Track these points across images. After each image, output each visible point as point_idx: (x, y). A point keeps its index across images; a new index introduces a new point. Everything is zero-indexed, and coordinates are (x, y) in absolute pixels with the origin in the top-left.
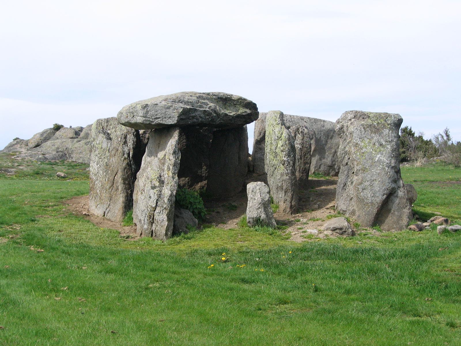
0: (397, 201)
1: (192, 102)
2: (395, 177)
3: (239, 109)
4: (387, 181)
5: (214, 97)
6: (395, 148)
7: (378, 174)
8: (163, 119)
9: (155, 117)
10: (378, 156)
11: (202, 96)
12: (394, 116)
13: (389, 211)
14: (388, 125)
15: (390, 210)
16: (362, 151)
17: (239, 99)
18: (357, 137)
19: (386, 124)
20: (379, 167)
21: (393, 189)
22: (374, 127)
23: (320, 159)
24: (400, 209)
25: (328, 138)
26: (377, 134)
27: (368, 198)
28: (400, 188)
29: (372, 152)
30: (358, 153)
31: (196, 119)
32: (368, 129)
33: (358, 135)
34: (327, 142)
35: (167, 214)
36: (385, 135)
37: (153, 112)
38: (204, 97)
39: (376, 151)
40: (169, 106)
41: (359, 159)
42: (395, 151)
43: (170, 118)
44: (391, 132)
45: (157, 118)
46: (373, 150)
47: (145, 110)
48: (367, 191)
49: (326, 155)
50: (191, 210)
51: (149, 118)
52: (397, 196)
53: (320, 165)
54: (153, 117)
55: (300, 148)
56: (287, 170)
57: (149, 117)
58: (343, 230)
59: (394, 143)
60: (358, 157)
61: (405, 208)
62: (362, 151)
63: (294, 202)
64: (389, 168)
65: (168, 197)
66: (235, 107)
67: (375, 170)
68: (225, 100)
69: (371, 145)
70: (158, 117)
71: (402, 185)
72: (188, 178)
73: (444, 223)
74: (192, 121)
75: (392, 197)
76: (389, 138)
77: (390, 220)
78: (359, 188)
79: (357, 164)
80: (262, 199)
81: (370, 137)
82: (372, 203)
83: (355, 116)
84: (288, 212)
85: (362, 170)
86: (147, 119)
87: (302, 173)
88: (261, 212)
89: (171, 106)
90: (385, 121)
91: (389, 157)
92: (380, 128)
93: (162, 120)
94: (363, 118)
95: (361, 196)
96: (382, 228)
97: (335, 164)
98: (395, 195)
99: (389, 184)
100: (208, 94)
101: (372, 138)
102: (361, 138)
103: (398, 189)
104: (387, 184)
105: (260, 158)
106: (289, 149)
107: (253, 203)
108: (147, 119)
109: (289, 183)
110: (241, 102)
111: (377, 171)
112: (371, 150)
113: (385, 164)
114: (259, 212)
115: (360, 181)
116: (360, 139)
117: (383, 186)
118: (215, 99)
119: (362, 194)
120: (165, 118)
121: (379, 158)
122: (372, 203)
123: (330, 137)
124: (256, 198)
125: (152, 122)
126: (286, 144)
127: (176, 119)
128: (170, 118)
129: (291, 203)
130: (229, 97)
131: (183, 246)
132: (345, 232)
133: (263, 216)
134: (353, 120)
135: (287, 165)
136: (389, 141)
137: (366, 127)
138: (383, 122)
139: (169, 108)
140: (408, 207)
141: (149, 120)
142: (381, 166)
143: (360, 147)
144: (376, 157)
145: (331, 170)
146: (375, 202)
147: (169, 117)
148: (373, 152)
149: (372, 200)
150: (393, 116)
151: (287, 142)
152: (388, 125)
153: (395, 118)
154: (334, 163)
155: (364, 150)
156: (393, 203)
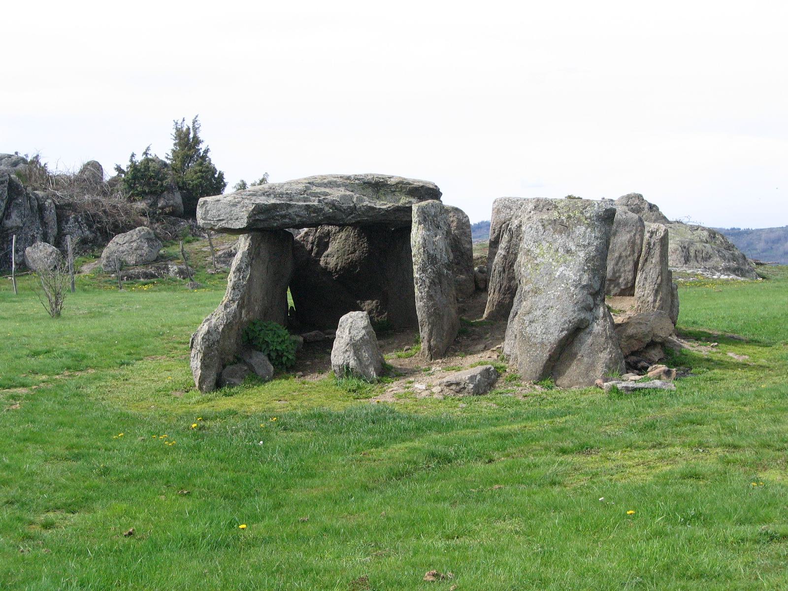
0: (589, 340)
1: (291, 193)
2: (588, 302)
3: (401, 198)
4: (571, 309)
6: (594, 257)
8: (228, 221)
9: (218, 219)
10: (561, 269)
11: (335, 182)
12: (598, 204)
13: (573, 356)
14: (586, 219)
15: (576, 354)
16: (535, 262)
17: (398, 183)
18: (531, 240)
20: (559, 287)
21: (581, 321)
22: (562, 223)
24: (593, 353)
26: (563, 234)
27: (537, 336)
28: (598, 319)
29: (551, 264)
30: (529, 266)
31: (290, 219)
32: (549, 227)
33: (532, 237)
35: (201, 360)
36: (577, 235)
37: (214, 211)
38: (338, 183)
39: (558, 262)
40: (235, 202)
41: (530, 274)
42: (593, 260)
43: (237, 219)
44: (589, 230)
45: (220, 220)
46: (553, 259)
47: (204, 209)
48: (536, 325)
50: (266, 353)
51: (210, 220)
52: (590, 333)
54: (215, 219)
55: (504, 255)
56: (421, 293)
57: (209, 218)
58: (462, 386)
59: (592, 248)
60: (529, 271)
61: (602, 352)
62: (535, 262)
63: (434, 341)
64: (576, 287)
65: (203, 335)
66: (394, 195)
67: (553, 291)
68: (378, 186)
69: (552, 251)
70: (221, 218)
71: (601, 315)
72: (376, 301)
73: (664, 377)
75: (582, 334)
76: (585, 241)
77: (574, 371)
78: (525, 320)
79: (526, 282)
80: (351, 337)
82: (542, 343)
83: (535, 207)
84: (426, 355)
85: (533, 291)
86: (206, 222)
87: (504, 294)
88: (349, 357)
89: (239, 202)
90: (582, 213)
91: (579, 271)
92: (571, 225)
93: (228, 223)
94: (548, 209)
95: (526, 333)
96: (558, 382)
97: (620, 277)
98: (587, 330)
99: (574, 313)
100: (348, 178)
101: (555, 240)
102: (537, 242)
103: (593, 320)
104: (571, 313)
106: (423, 261)
107: (339, 343)
108: (206, 222)
109: (424, 312)
110: (401, 187)
111: (556, 293)
112: (551, 260)
113: (570, 281)
114: (346, 356)
115: (528, 309)
116: (534, 242)
117: (562, 317)
118: (358, 185)
119: (528, 329)
120: (231, 219)
121: (562, 273)
122: (542, 343)
124: (344, 336)
125: (214, 225)
126: (419, 253)
127: (246, 221)
128: (237, 219)
129: (429, 341)
130: (381, 180)
131: (223, 403)
132: (464, 388)
133: (352, 363)
134: (532, 212)
135: (420, 286)
136: (584, 245)
138: (578, 215)
139: (235, 205)
140: (608, 350)
141: (210, 223)
142: (563, 285)
143: (533, 255)
144: (557, 270)
145: (612, 286)
146: (546, 342)
147: (235, 218)
148: (554, 263)
149: (542, 339)
150: (596, 206)
151: (422, 250)
152: (586, 219)
153: (599, 207)
154: (617, 274)
155: (539, 260)
156: (582, 344)
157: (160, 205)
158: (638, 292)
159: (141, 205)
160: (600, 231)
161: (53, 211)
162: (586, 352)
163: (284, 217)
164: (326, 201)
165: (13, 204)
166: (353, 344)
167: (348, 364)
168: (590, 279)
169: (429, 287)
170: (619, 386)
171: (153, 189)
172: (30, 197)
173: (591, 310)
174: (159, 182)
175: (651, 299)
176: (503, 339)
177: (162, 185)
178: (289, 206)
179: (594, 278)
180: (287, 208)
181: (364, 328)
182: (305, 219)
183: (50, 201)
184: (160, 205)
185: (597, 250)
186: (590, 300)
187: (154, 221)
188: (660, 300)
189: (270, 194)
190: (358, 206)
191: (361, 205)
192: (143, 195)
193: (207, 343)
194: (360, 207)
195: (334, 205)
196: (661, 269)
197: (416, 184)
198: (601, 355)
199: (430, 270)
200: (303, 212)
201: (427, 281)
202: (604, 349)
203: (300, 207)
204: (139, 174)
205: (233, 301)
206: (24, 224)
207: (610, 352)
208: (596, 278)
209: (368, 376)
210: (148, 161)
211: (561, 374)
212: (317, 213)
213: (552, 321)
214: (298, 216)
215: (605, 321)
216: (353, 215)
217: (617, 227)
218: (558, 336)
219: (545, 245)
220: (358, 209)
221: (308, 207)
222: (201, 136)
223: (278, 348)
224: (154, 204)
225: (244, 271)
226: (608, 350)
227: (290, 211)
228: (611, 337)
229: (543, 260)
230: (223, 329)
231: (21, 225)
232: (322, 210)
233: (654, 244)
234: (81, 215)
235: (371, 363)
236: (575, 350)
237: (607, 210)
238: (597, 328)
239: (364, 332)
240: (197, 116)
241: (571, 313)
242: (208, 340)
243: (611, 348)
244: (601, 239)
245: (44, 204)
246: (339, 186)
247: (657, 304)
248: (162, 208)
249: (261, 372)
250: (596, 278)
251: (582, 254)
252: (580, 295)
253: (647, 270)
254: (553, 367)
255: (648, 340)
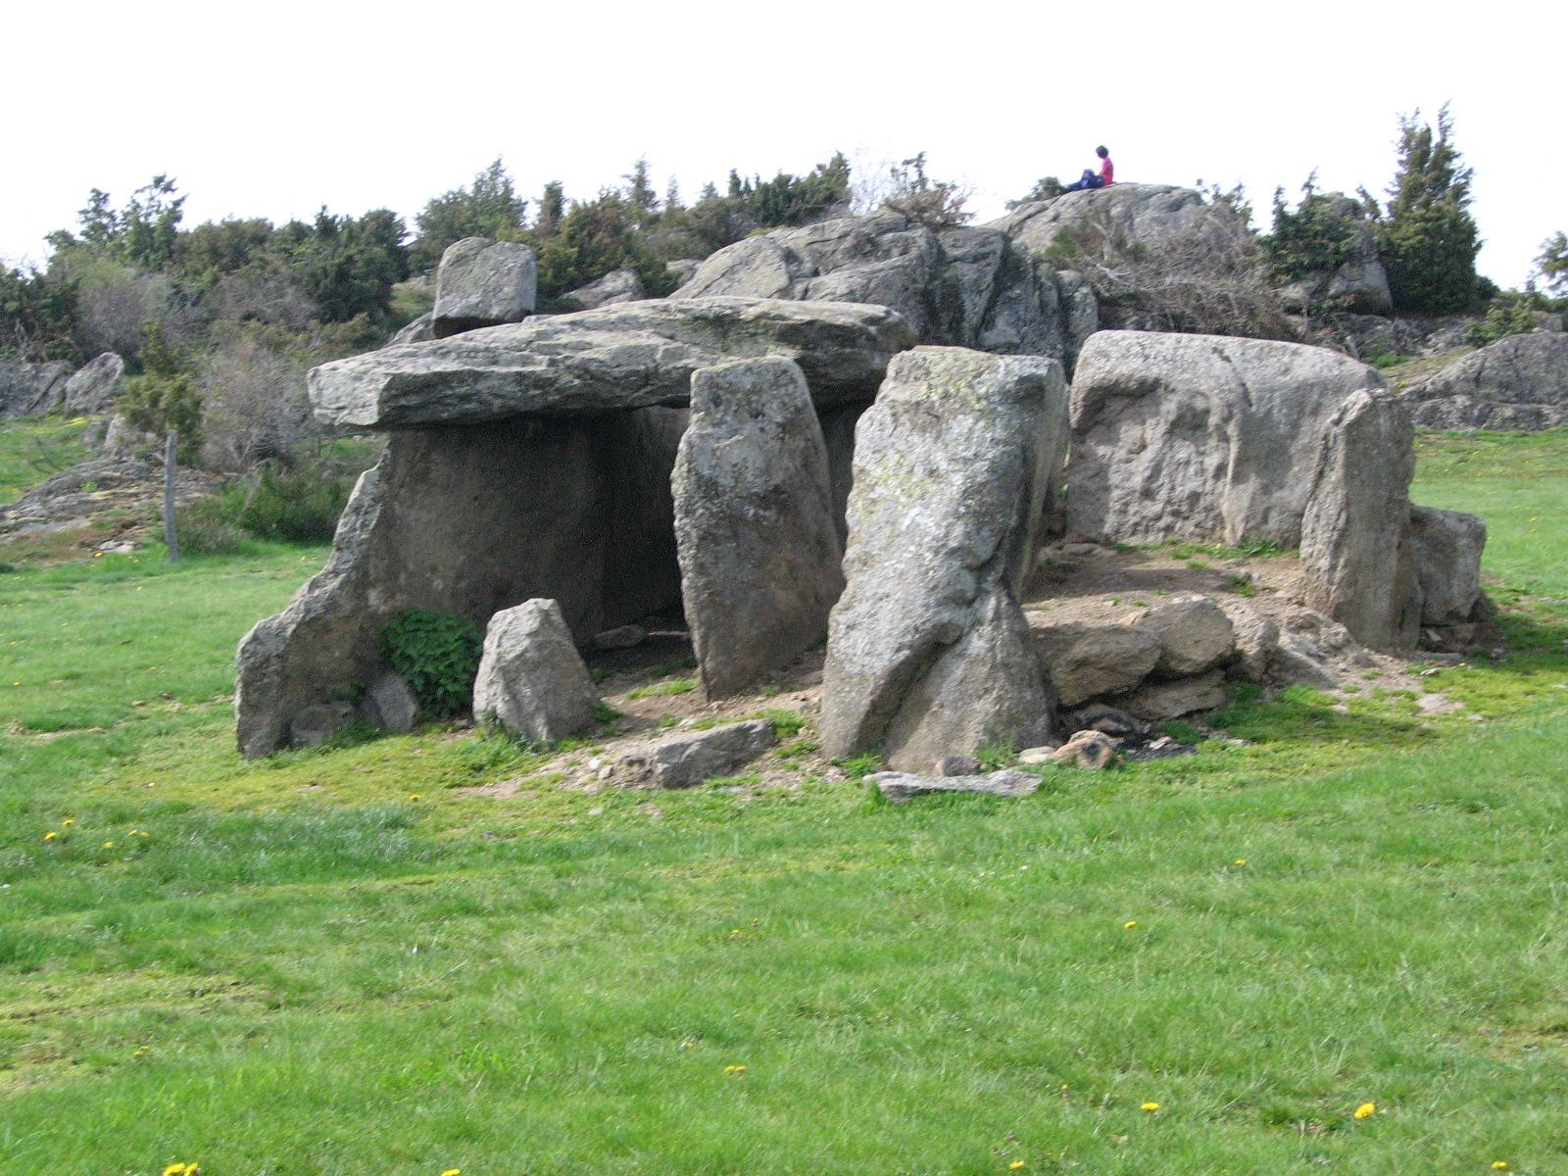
0: (959, 670)
5: (680, 316)
6: (983, 484)
7: (902, 574)
10: (914, 512)
13: (924, 705)
14: (979, 399)
15: (928, 702)
19: (972, 399)
21: (942, 628)
23: (1266, 490)
24: (964, 698)
25: (1301, 413)
28: (982, 624)
30: (860, 503)
34: (1295, 426)
39: (910, 496)
42: (979, 492)
44: (982, 424)
49: (1291, 474)
50: (407, 677)
53: (1267, 511)
59: (982, 466)
64: (936, 552)
69: (902, 473)
70: (341, 404)
71: (990, 615)
74: (457, 409)
75: (947, 657)
77: (924, 736)
81: (902, 447)
82: (862, 675)
90: (970, 386)
91: (945, 517)
96: (892, 762)
98: (959, 648)
101: (911, 448)
102: (879, 451)
104: (920, 611)
105: (1080, 487)
112: (898, 492)
117: (903, 619)
118: (684, 323)
119: (843, 643)
123: (1308, 409)
130: (728, 312)
137: (900, 409)
138: (964, 390)
140: (995, 694)
152: (979, 399)
153: (1007, 373)
156: (945, 678)
157: (1332, 292)
158: (1305, 549)
159: (1295, 292)
160: (1006, 427)
161: (1089, 311)
162: (951, 698)
163: (465, 398)
164: (569, 362)
165: (1001, 299)
166: (501, 668)
167: (494, 710)
168: (967, 535)
169: (698, 547)
170: (884, 784)
171: (1320, 259)
172: (1042, 285)
173: (970, 603)
174: (1332, 245)
175: (1324, 563)
176: (821, 667)
177: (1337, 251)
178: (477, 376)
179: (978, 531)
180: (476, 381)
181: (529, 635)
182: (512, 403)
183: (1085, 290)
184: (1332, 292)
185: (992, 470)
186: (968, 581)
187: (1320, 323)
188: (1345, 566)
189: (449, 352)
190: (662, 370)
191: (671, 366)
192: (1296, 273)
193: (252, 660)
194: (668, 372)
195: (587, 371)
196: (1347, 496)
197: (796, 317)
198: (978, 706)
199: (701, 511)
200: (511, 388)
201: (694, 534)
202: (987, 691)
203: (504, 377)
204: (1291, 229)
205: (335, 573)
206: (1023, 339)
207: (999, 699)
208: (985, 533)
209: (531, 734)
210: (1313, 201)
211: (900, 743)
212: (541, 387)
213: (883, 627)
214: (496, 396)
215: (996, 628)
216: (649, 388)
217: (1322, 395)
218: (890, 660)
219: (893, 458)
220: (664, 374)
221: (520, 377)
222: (1455, 142)
223: (429, 669)
224: (1320, 291)
225: (366, 513)
226: (995, 694)
227: (481, 386)
228: (1006, 666)
229: (885, 492)
230: (295, 631)
231: (1017, 340)
232: (552, 382)
233: (1335, 438)
234: (1152, 318)
235: (537, 709)
236: (929, 691)
237: (1022, 380)
238: (977, 644)
239: (526, 642)
240: (1447, 103)
241: (920, 611)
242: (254, 654)
243: (1002, 688)
244: (1006, 443)
245: (1072, 297)
246: (642, 326)
247: (1338, 575)
248: (1335, 297)
249: (393, 718)
250: (985, 533)
251: (958, 479)
252: (940, 570)
253: (1321, 497)
254: (886, 729)
255: (1147, 667)
